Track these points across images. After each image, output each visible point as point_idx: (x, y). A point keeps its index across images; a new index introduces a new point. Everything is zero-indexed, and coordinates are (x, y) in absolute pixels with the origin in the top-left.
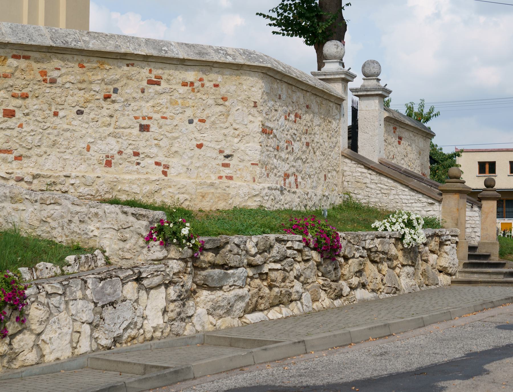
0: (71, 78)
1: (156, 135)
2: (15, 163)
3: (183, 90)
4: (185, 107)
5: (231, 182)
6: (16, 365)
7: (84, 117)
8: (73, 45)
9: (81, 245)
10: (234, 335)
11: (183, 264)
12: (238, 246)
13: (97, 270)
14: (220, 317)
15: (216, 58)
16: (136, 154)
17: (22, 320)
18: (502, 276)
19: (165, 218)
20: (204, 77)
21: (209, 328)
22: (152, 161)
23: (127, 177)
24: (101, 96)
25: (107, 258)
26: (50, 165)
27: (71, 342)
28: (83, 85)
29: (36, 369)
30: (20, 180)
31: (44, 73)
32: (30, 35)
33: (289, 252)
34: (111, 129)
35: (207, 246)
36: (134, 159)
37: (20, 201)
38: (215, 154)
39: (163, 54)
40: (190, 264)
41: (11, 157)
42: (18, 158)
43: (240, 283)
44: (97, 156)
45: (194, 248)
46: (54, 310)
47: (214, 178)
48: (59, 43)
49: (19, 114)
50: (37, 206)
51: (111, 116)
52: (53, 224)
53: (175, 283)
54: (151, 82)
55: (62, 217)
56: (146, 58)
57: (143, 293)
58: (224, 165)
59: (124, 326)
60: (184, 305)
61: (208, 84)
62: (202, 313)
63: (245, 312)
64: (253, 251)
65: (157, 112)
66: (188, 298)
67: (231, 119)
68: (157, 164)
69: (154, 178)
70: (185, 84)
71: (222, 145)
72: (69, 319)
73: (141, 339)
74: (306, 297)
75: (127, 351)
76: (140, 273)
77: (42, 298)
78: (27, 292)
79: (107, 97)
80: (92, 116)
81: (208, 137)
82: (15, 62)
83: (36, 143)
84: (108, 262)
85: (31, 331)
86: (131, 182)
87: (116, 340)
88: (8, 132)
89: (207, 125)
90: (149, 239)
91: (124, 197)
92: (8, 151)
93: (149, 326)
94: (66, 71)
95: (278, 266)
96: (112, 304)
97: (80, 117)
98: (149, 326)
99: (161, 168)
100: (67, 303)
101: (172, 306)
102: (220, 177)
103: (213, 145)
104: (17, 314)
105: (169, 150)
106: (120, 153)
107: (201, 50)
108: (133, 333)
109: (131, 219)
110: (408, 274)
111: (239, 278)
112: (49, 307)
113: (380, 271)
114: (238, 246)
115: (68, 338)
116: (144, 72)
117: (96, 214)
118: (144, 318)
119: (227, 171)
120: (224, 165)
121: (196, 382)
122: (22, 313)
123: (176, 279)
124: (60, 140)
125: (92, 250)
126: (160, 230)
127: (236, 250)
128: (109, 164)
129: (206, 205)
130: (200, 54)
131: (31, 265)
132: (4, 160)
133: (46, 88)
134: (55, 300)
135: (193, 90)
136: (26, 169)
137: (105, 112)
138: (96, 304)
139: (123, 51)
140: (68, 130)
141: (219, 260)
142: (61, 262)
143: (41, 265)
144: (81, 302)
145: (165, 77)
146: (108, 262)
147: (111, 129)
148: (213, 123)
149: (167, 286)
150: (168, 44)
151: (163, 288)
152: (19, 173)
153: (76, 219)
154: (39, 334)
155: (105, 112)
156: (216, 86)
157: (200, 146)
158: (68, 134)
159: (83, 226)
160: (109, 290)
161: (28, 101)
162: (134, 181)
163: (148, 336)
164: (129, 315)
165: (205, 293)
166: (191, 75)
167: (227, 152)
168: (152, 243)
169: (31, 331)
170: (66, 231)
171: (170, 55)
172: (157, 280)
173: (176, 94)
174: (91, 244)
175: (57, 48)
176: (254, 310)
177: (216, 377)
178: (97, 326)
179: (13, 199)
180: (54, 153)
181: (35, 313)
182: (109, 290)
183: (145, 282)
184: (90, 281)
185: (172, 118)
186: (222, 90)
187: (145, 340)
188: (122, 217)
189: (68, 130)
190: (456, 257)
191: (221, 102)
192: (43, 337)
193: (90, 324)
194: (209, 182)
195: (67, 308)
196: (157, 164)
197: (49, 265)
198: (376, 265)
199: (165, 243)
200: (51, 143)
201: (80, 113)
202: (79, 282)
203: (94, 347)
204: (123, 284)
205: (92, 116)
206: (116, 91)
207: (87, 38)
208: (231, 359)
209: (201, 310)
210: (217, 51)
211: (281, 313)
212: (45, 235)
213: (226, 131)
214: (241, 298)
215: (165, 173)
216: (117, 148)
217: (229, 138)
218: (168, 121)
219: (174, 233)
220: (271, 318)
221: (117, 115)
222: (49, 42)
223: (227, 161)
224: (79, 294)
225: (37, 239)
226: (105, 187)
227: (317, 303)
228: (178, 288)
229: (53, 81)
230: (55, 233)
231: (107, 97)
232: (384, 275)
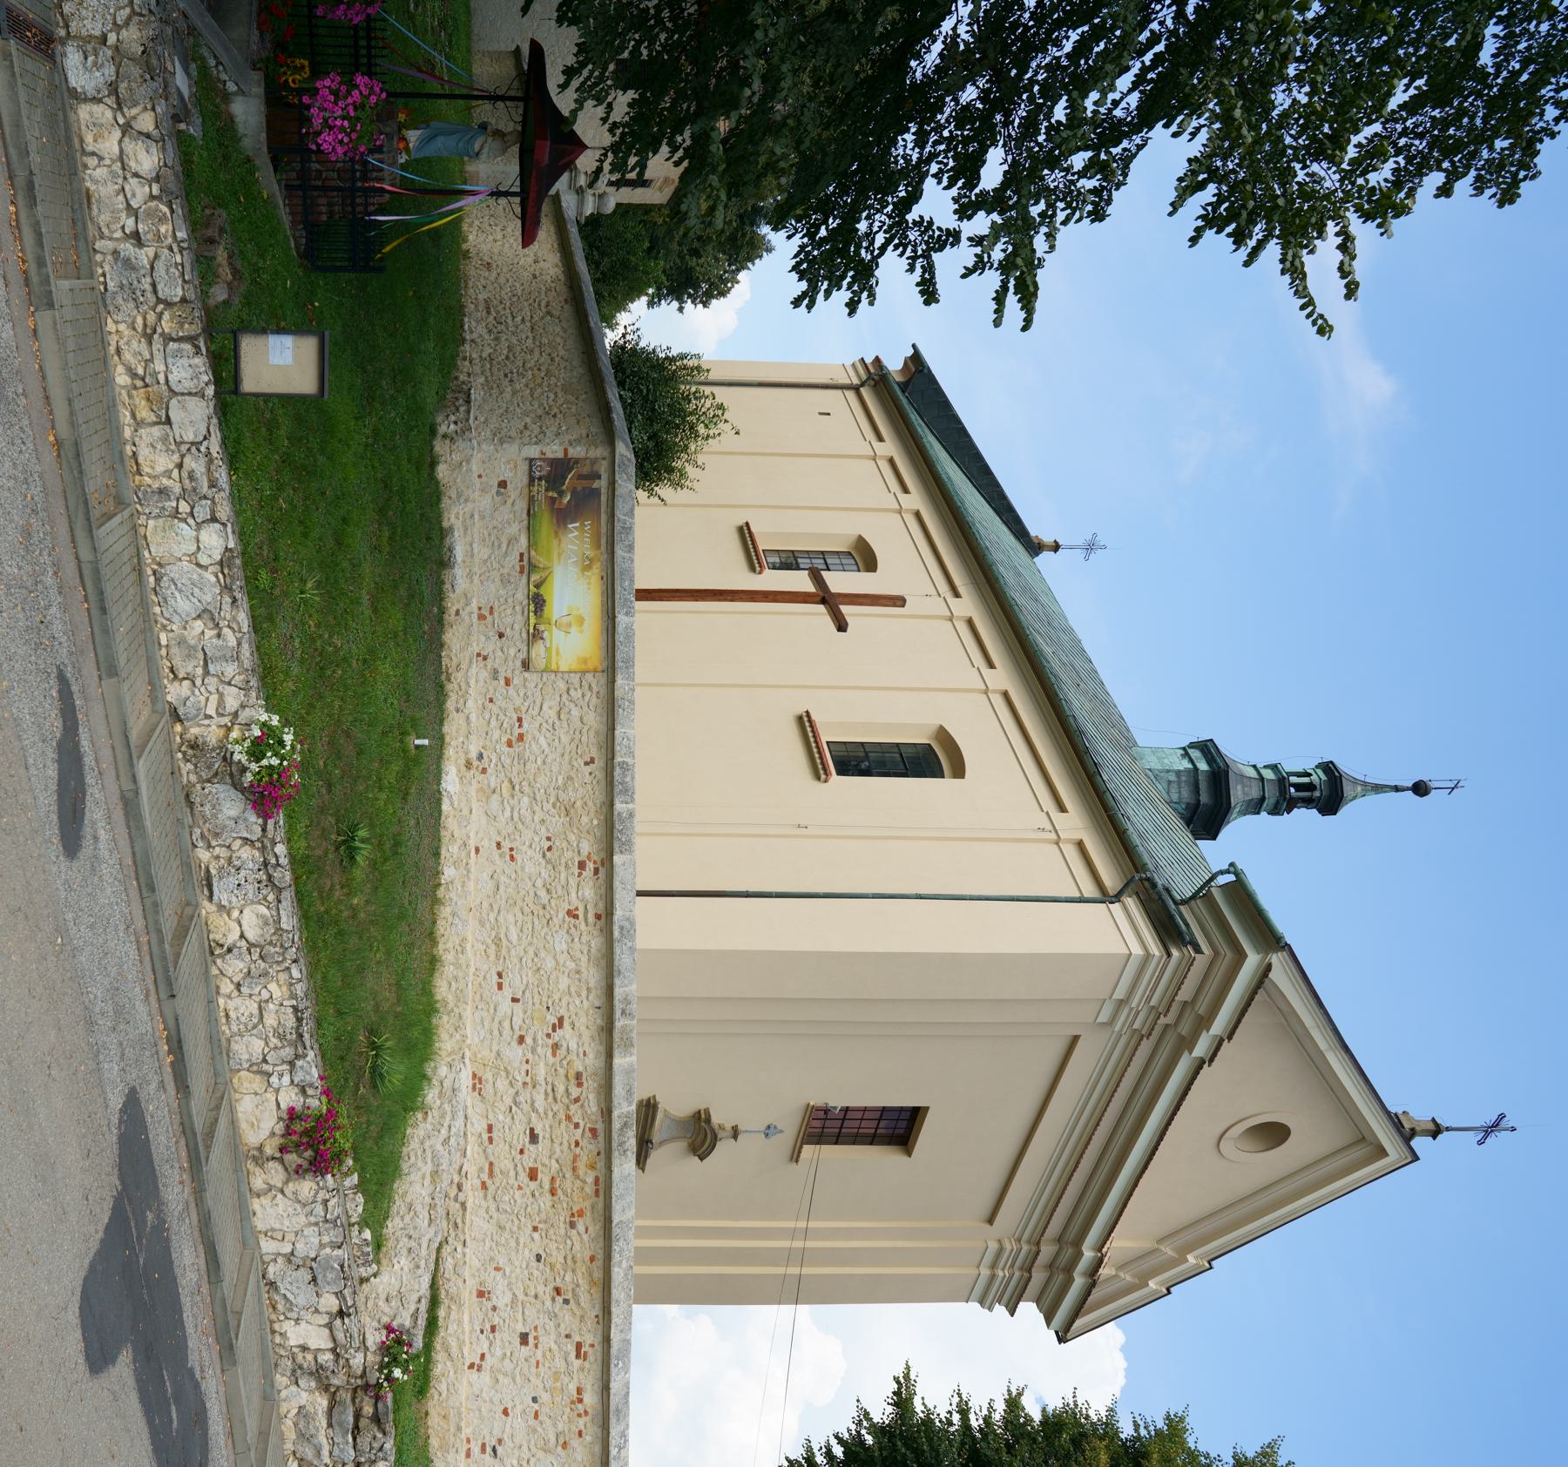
0: (577, 1247)
1: (516, 1354)
2: (478, 1183)
3: (572, 1388)
4: (552, 1391)
5: (463, 1455)
6: (251, 1166)
7: (534, 1263)
8: (615, 1247)
9: (384, 1249)
10: (273, 1439)
11: (359, 1373)
12: (381, 1449)
13: (354, 1266)
14: (296, 1425)
15: (614, 1432)
16: (493, 1329)
17: (299, 1172)
19: (413, 1351)
20: (589, 1418)
21: (284, 1408)
22: (486, 1350)
23: (466, 1318)
24: (559, 1283)
25: (367, 1280)
26: (478, 1223)
27: (273, 1230)
28: (571, 1261)
29: (244, 1188)
30: (460, 1187)
31: (581, 1213)
32: (622, 1195)
34: (521, 1297)
35: (380, 1405)
36: (488, 1326)
37: (433, 1182)
38: (497, 1433)
39: (614, 1361)
40: (359, 1382)
41: (485, 1177)
42: (484, 1186)
43: (336, 1452)
44: (489, 1280)
45: (379, 1386)
46: (308, 1209)
47: (467, 1432)
48: (616, 1231)
49: (533, 1185)
50: (428, 1200)
51: (536, 1297)
52: (407, 1219)
53: (337, 1361)
54: (579, 1346)
55: (415, 1228)
56: (607, 1340)
57: (325, 1319)
58: (484, 1446)
59: (289, 1295)
60: (311, 1374)
61: (581, 1421)
62: (300, 1398)
65: (544, 1356)
66: (319, 1379)
67: (540, 1454)
68: (483, 1356)
69: (466, 1352)
70: (579, 1391)
71: (508, 1442)
72: (298, 1227)
73: (274, 1317)
75: (260, 1299)
76: (349, 1315)
77: (322, 1195)
78: (329, 1176)
79: (558, 1291)
80: (536, 1273)
81: (517, 1422)
82: (590, 1180)
83: (502, 1206)
84: (363, 1280)
85: (286, 1182)
86: (460, 1323)
87: (272, 1284)
88: (512, 1173)
89: (532, 1422)
90: (389, 1329)
91: (442, 1313)
92: (491, 1174)
93: (288, 1327)
94: (583, 1242)
96: (314, 1279)
97: (533, 1259)
98: (288, 1327)
99: (477, 1361)
100: (316, 1224)
101: (310, 1357)
102: (468, 1441)
103: (508, 1430)
104: (305, 1165)
105: (499, 1371)
106: (494, 1309)
107: (623, 1413)
108: (280, 1307)
109: (413, 1308)
111: (342, 1451)
114: (381, 1449)
115: (277, 1226)
116: (590, 1338)
117: (418, 1267)
118: (297, 1321)
119: (476, 1450)
120: (484, 1445)
121: (219, 1371)
122: (307, 1171)
123: (342, 1362)
124: (506, 1235)
125: (378, 1263)
126: (399, 1342)
127: (376, 1445)
128: (481, 1294)
129: (434, 1421)
130: (618, 1411)
131: (361, 1187)
132: (481, 1170)
133: (564, 1216)
134: (319, 1209)
135: (573, 1402)
136: (472, 1196)
137: (541, 1289)
138: (314, 1260)
139: (613, 1309)
140: (518, 1243)
141: (363, 1423)
142: (364, 1223)
143: (360, 1199)
144: (316, 1241)
145: (587, 1364)
146: (363, 1280)
147: (521, 1297)
148: (535, 1431)
149: (333, 1350)
150: (626, 1369)
151: (331, 1345)
152: (467, 1186)
153: (413, 1244)
154: (282, 1192)
155: (541, 1289)
156: (580, 1434)
157: (505, 1412)
158: (513, 1244)
159: (404, 1252)
160: (330, 1276)
161: (548, 1196)
162: (461, 1327)
163: (276, 1326)
164: (301, 1301)
165: (325, 1403)
166: (591, 1399)
167: (499, 1449)
168: (384, 1332)
169: (286, 1182)
170: (399, 1233)
171: (613, 1371)
172: (340, 1336)
173: (566, 1380)
174: (384, 1262)
175: (610, 1229)
177: (223, 1400)
178: (290, 1261)
179: (435, 1173)
180: (490, 1228)
181: (306, 1187)
182: (330, 1276)
183: (338, 1321)
184: (339, 1252)
185: (538, 1375)
186: (575, 1442)
187: (272, 1322)
188: (415, 1297)
189: (518, 1243)
191: (561, 1441)
192: (280, 1196)
193: (292, 1253)
194: (463, 1424)
195: (310, 1224)
196: (483, 1356)
197: (360, 1209)
199: (384, 1349)
200: (503, 1223)
201: (539, 1258)
202: (340, 1239)
203: (267, 1259)
205: (536, 1273)
206: (566, 1302)
207: (624, 1264)
208: (243, 1421)
209: (304, 1397)
210: (624, 1435)
212: (394, 1209)
213: (525, 1448)
214: (318, 1453)
215: (471, 1366)
216: (500, 1305)
217: (516, 1452)
218: (533, 1370)
219: (395, 1360)
221: (538, 1304)
222: (616, 1219)
223: (489, 1450)
224: (326, 1239)
225: (391, 1200)
226: (453, 1290)
228: (331, 1365)
229: (572, 1225)
230: (397, 1220)
231: (558, 1291)
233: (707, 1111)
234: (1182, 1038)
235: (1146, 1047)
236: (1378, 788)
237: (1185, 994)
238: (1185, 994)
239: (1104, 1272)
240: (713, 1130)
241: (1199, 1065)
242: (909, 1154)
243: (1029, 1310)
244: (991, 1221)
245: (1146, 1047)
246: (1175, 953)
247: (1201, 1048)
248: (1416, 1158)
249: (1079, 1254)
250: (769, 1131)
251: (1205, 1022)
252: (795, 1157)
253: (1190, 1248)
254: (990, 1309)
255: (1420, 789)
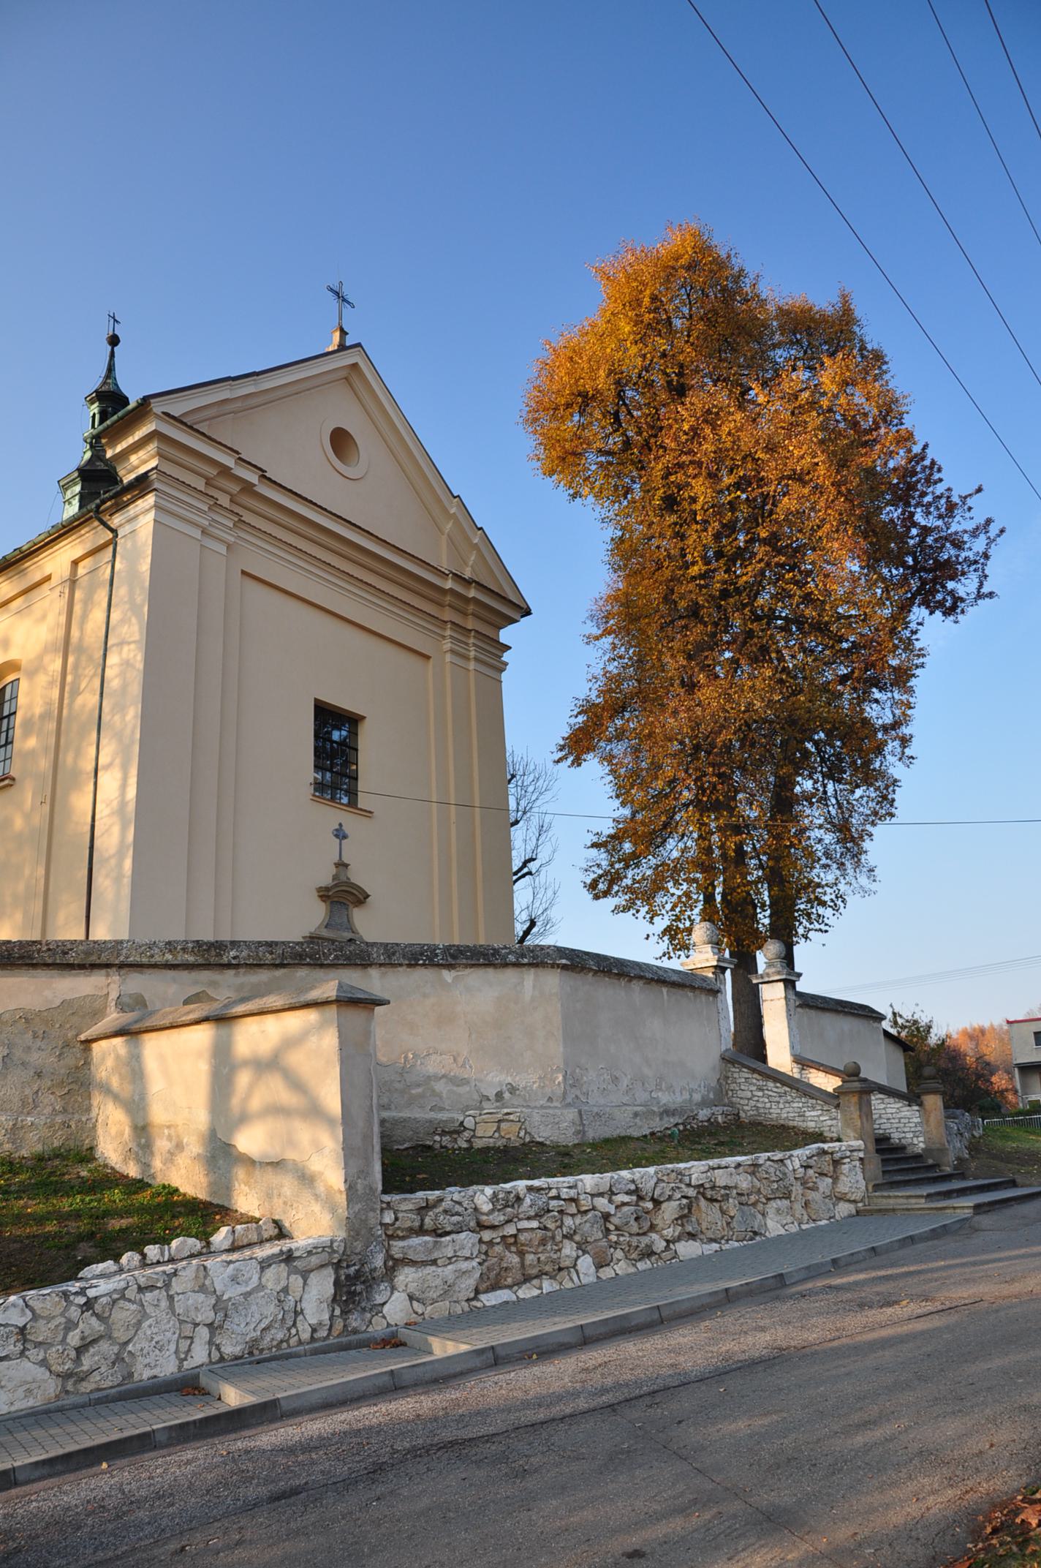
18: (923, 1201)
27: (177, 1352)
33: (553, 1203)
63: (477, 1292)
64: (486, 1207)
73: (293, 1341)
74: (586, 1263)
95: (535, 1224)
110: (778, 1210)
112: (142, 1305)
113: (723, 1212)
115: (173, 1347)
165: (407, 1270)
176: (494, 1287)
187: (300, 1343)
190: (860, 1177)
192: (130, 1347)
198: (717, 1205)
204: (262, 1269)
211: (541, 1288)
220: (522, 1296)
227: (607, 1269)
232: (732, 1218)
233: (319, 889)
234: (243, 490)
235: (248, 517)
236: (111, 369)
237: (200, 484)
238: (200, 484)
239: (467, 574)
240: (336, 885)
241: (263, 477)
242: (364, 718)
243: (505, 635)
244: (428, 658)
245: (248, 517)
246: (156, 485)
247: (253, 478)
248: (359, 345)
249: (474, 599)
250: (340, 834)
251: (225, 471)
252: (368, 813)
253: (446, 511)
254: (506, 664)
255: (114, 341)
